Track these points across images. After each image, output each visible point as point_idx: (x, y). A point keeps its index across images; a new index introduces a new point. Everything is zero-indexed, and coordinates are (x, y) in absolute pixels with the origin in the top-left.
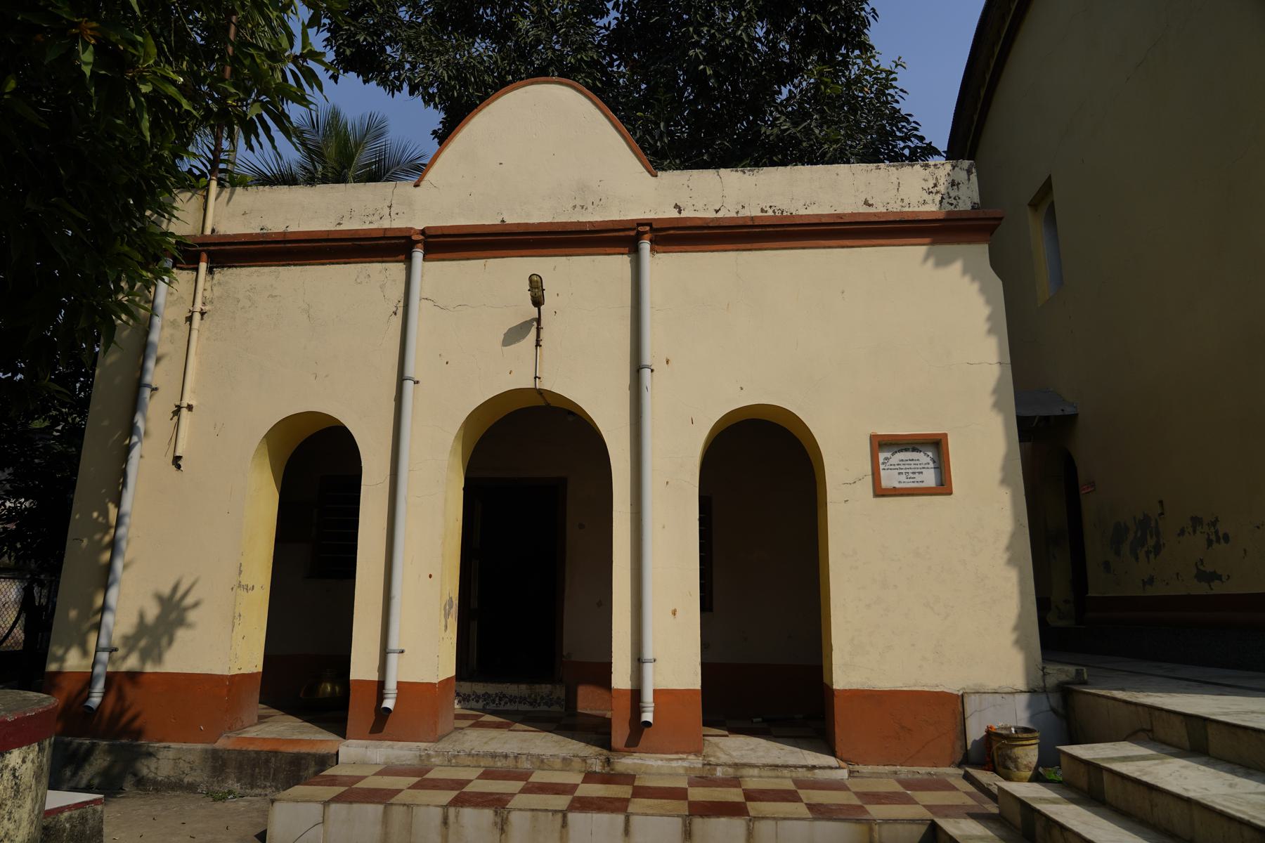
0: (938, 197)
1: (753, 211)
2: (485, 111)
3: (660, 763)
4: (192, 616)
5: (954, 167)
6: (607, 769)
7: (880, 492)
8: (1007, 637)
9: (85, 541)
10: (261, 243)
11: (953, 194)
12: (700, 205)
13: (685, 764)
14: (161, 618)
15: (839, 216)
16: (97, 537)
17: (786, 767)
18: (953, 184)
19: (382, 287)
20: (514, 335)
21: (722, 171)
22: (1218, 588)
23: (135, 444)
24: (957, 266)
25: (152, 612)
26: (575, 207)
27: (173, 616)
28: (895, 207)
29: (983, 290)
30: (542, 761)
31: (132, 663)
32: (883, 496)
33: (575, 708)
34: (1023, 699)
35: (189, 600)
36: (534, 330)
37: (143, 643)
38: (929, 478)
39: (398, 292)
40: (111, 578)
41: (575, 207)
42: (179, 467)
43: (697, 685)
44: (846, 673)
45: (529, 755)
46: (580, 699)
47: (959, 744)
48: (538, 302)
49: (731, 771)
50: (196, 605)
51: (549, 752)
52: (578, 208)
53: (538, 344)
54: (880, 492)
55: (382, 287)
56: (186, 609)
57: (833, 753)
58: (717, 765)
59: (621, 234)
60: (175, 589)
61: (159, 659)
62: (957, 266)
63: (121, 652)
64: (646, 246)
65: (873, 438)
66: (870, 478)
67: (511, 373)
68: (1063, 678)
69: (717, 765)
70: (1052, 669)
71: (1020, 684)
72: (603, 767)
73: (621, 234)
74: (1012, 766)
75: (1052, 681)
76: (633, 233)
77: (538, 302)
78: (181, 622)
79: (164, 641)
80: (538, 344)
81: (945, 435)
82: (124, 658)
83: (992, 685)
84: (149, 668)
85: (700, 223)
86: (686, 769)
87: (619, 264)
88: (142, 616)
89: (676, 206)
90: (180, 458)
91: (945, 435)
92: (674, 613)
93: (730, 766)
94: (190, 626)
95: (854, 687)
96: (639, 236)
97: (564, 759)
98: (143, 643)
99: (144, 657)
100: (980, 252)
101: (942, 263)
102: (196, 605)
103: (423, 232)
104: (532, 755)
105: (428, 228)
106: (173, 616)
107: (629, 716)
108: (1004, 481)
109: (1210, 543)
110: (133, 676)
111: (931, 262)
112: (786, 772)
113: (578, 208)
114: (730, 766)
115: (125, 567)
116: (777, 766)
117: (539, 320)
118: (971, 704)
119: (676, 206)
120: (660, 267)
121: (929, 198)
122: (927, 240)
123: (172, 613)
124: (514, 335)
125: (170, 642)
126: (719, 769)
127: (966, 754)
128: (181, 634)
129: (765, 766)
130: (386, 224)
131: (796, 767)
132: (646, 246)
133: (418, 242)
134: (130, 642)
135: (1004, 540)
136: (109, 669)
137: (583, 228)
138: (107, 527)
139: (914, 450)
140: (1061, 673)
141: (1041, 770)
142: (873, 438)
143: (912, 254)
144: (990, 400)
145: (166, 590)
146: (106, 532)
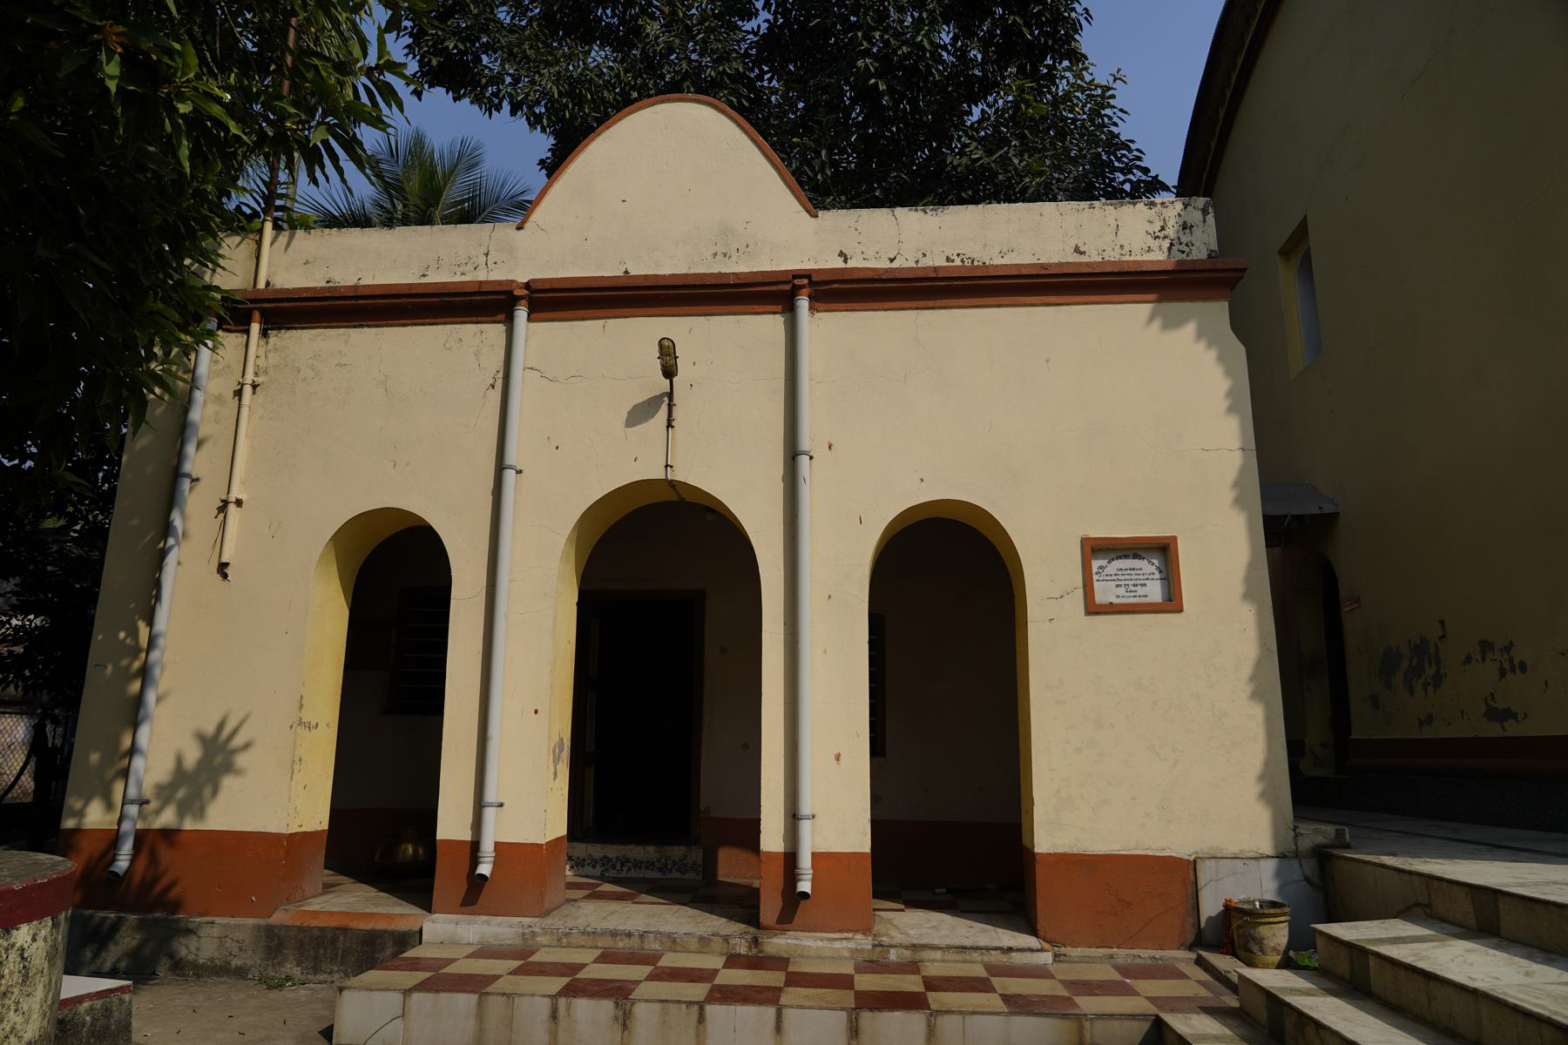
0: (1166, 243)
1: (936, 260)
3: (820, 943)
4: (241, 760)
6: (754, 951)
7: (1093, 609)
8: (1251, 788)
9: (110, 668)
11: (1184, 239)
12: (870, 253)
13: (851, 945)
14: (203, 763)
15: (1043, 266)
16: (124, 662)
18: (1185, 226)
20: (640, 413)
21: (898, 210)
22: (1513, 729)
23: (171, 548)
24: (1190, 329)
27: (219, 760)
28: (1113, 255)
29: (1221, 358)
30: (674, 941)
31: (167, 818)
34: (1270, 866)
35: (238, 741)
36: (664, 408)
37: (181, 794)
38: (1154, 592)
40: (141, 715)
42: (225, 576)
45: (657, 933)
47: (1190, 920)
48: (669, 372)
49: (907, 953)
50: (247, 746)
53: (670, 425)
54: (1093, 609)
56: (234, 752)
57: (1034, 932)
59: (773, 288)
61: (201, 814)
62: (1190, 329)
63: (153, 805)
64: (803, 303)
66: (1080, 592)
67: (635, 460)
68: (1320, 839)
71: (1267, 847)
72: (750, 948)
73: (773, 288)
74: (1255, 948)
75: (1305, 844)
76: (787, 287)
77: (669, 372)
78: (228, 768)
79: (207, 791)
80: (670, 425)
82: (158, 812)
84: (189, 825)
86: (852, 951)
88: (179, 760)
89: (841, 254)
90: (226, 565)
92: (838, 758)
93: (906, 947)
94: (239, 772)
95: (1061, 850)
97: (701, 938)
98: (181, 794)
99: (182, 811)
100: (1219, 311)
101: (1170, 324)
102: (247, 746)
103: (527, 286)
106: (219, 760)
109: (1503, 673)
110: (168, 835)
111: (1157, 324)
112: (975, 955)
114: (906, 947)
115: (159, 700)
116: (965, 948)
117: (670, 395)
118: (1205, 873)
119: (841, 254)
120: (821, 329)
121: (1155, 244)
122: (1153, 297)
123: (217, 756)
124: (640, 413)
125: (215, 791)
126: (892, 951)
128: (228, 782)
129: (949, 947)
130: (482, 276)
131: (988, 949)
132: (803, 303)
133: (521, 298)
134: (165, 792)
136: (139, 826)
138: (136, 651)
139: (1136, 556)
140: (1318, 833)
141: (1291, 953)
143: (1133, 315)
145: (209, 728)
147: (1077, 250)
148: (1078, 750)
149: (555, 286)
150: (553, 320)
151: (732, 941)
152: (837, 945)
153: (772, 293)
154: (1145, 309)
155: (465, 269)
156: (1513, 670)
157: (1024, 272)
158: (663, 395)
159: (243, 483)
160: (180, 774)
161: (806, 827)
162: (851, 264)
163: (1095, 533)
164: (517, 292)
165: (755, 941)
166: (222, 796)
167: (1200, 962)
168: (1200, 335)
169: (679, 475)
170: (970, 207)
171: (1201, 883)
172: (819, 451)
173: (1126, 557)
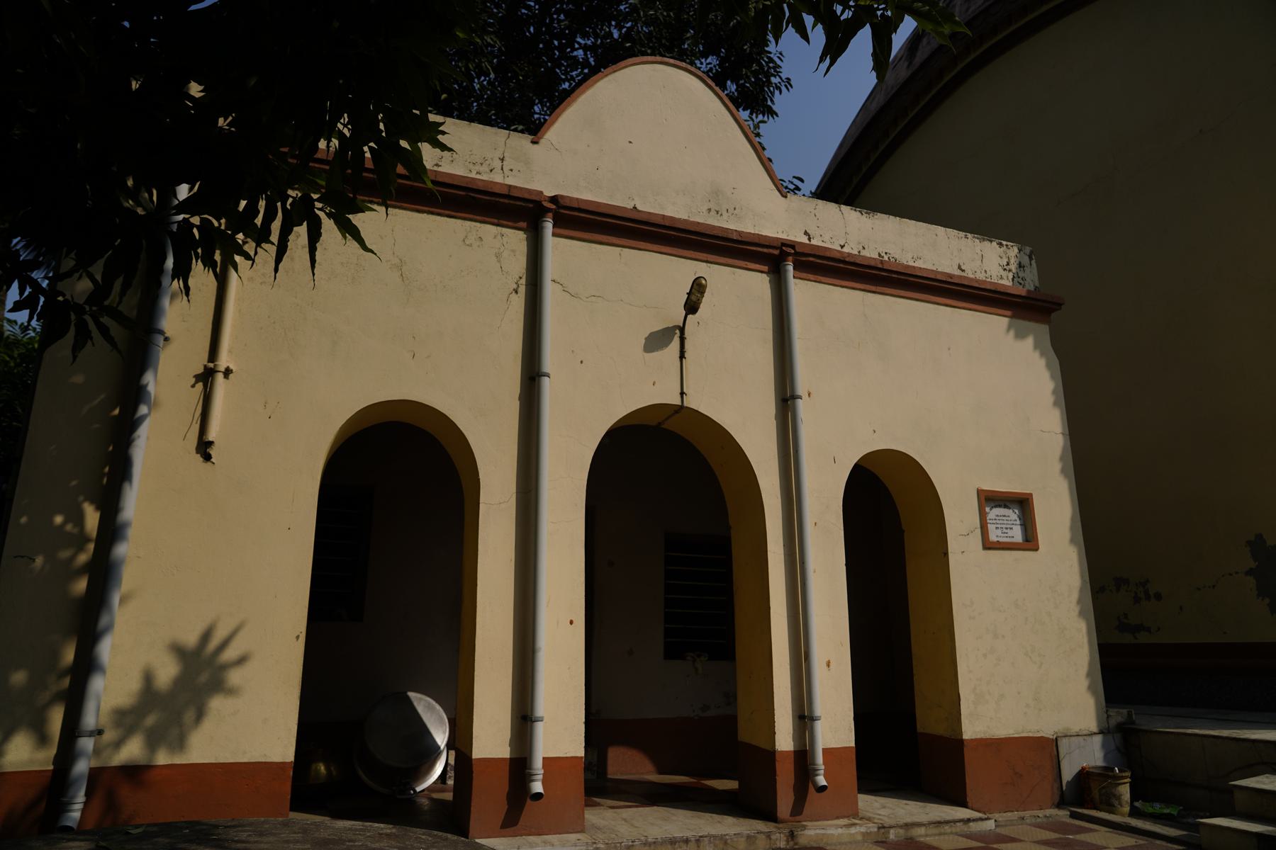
0: (1011, 276)
1: (871, 253)
2: (610, 77)
3: (840, 831)
4: (235, 677)
5: (1020, 250)
6: (791, 843)
7: (988, 545)
8: (1084, 683)
9: (39, 561)
10: (814, 256)
11: (1021, 274)
12: (826, 238)
13: (863, 830)
14: (181, 682)
15: (936, 272)
16: (65, 554)
17: (947, 822)
18: (1020, 266)
19: (498, 256)
20: (656, 341)
21: (843, 207)
22: (1143, 638)
23: (143, 418)
24: (1030, 341)
25: (167, 672)
26: (709, 210)
27: (204, 678)
28: (981, 276)
29: (1048, 366)
30: (726, 843)
31: (132, 750)
32: (990, 549)
33: (605, 773)
34: (1098, 739)
35: (230, 654)
36: (676, 340)
37: (150, 720)
38: (1017, 535)
39: (518, 265)
40: (103, 621)
41: (709, 210)
42: (207, 457)
43: (853, 744)
44: (977, 723)
45: (710, 836)
46: (610, 762)
47: (1056, 785)
48: (692, 307)
49: (901, 831)
50: (242, 660)
51: (732, 831)
52: (713, 213)
53: (682, 356)
54: (988, 545)
55: (498, 256)
56: (225, 667)
57: (964, 805)
58: (891, 827)
59: (765, 250)
60: (206, 636)
61: (180, 744)
62: (1030, 341)
63: (109, 736)
64: (549, 226)
65: (980, 492)
66: (978, 531)
67: (648, 385)
68: (1120, 719)
69: (891, 827)
70: (1112, 712)
71: (1093, 727)
72: (787, 841)
73: (765, 250)
74: (1116, 803)
75: (1113, 722)
76: (776, 252)
77: (692, 307)
78: (217, 685)
79: (189, 716)
80: (682, 356)
81: (1031, 495)
82: (118, 744)
83: (1075, 728)
84: (162, 758)
85: (645, 218)
86: (864, 834)
87: (510, 243)
88: (148, 678)
89: (806, 233)
90: (211, 443)
91: (1031, 495)
92: (828, 664)
93: (901, 827)
94: (232, 692)
95: (979, 736)
96: (783, 257)
97: (749, 837)
98: (150, 720)
99: (154, 740)
100: (1044, 329)
101: (1020, 335)
102: (242, 660)
103: (554, 199)
104: (714, 836)
105: (562, 197)
106: (204, 678)
107: (792, 782)
108: (1072, 541)
109: (1137, 600)
110: (133, 772)
111: (1012, 333)
112: (947, 828)
113: (713, 213)
114: (901, 827)
115: (122, 601)
116: (940, 823)
117: (682, 330)
118: (1064, 745)
119: (806, 233)
120: (561, 252)
121: (1004, 274)
122: (1009, 313)
123: (202, 673)
124: (656, 341)
125: (200, 715)
126: (892, 831)
127: (1062, 794)
128: (217, 704)
129: (931, 823)
130: (498, 178)
131: (955, 822)
132: (549, 226)
133: (549, 210)
134: (127, 720)
135: (1075, 595)
136: (94, 764)
137: (730, 236)
138: (82, 539)
139: (1006, 507)
140: (1119, 715)
141: (1137, 804)
142: (980, 492)
143: (995, 324)
144: (1058, 466)
145: (190, 638)
146: (81, 548)
147: (959, 267)
148: (985, 655)
149: (653, 220)
150: (432, 213)
151: (773, 837)
152: (853, 830)
153: (772, 257)
154: (1006, 320)
155: (481, 169)
156: (1148, 597)
157: (939, 277)
158: (678, 327)
159: (230, 351)
160: (149, 695)
161: (540, 730)
162: (814, 242)
163: (987, 486)
164: (547, 204)
165: (792, 835)
166: (208, 725)
167: (1074, 815)
168: (1036, 346)
169: (691, 402)
170: (477, 127)
171: (1061, 756)
172: (805, 396)
173: (1000, 506)
